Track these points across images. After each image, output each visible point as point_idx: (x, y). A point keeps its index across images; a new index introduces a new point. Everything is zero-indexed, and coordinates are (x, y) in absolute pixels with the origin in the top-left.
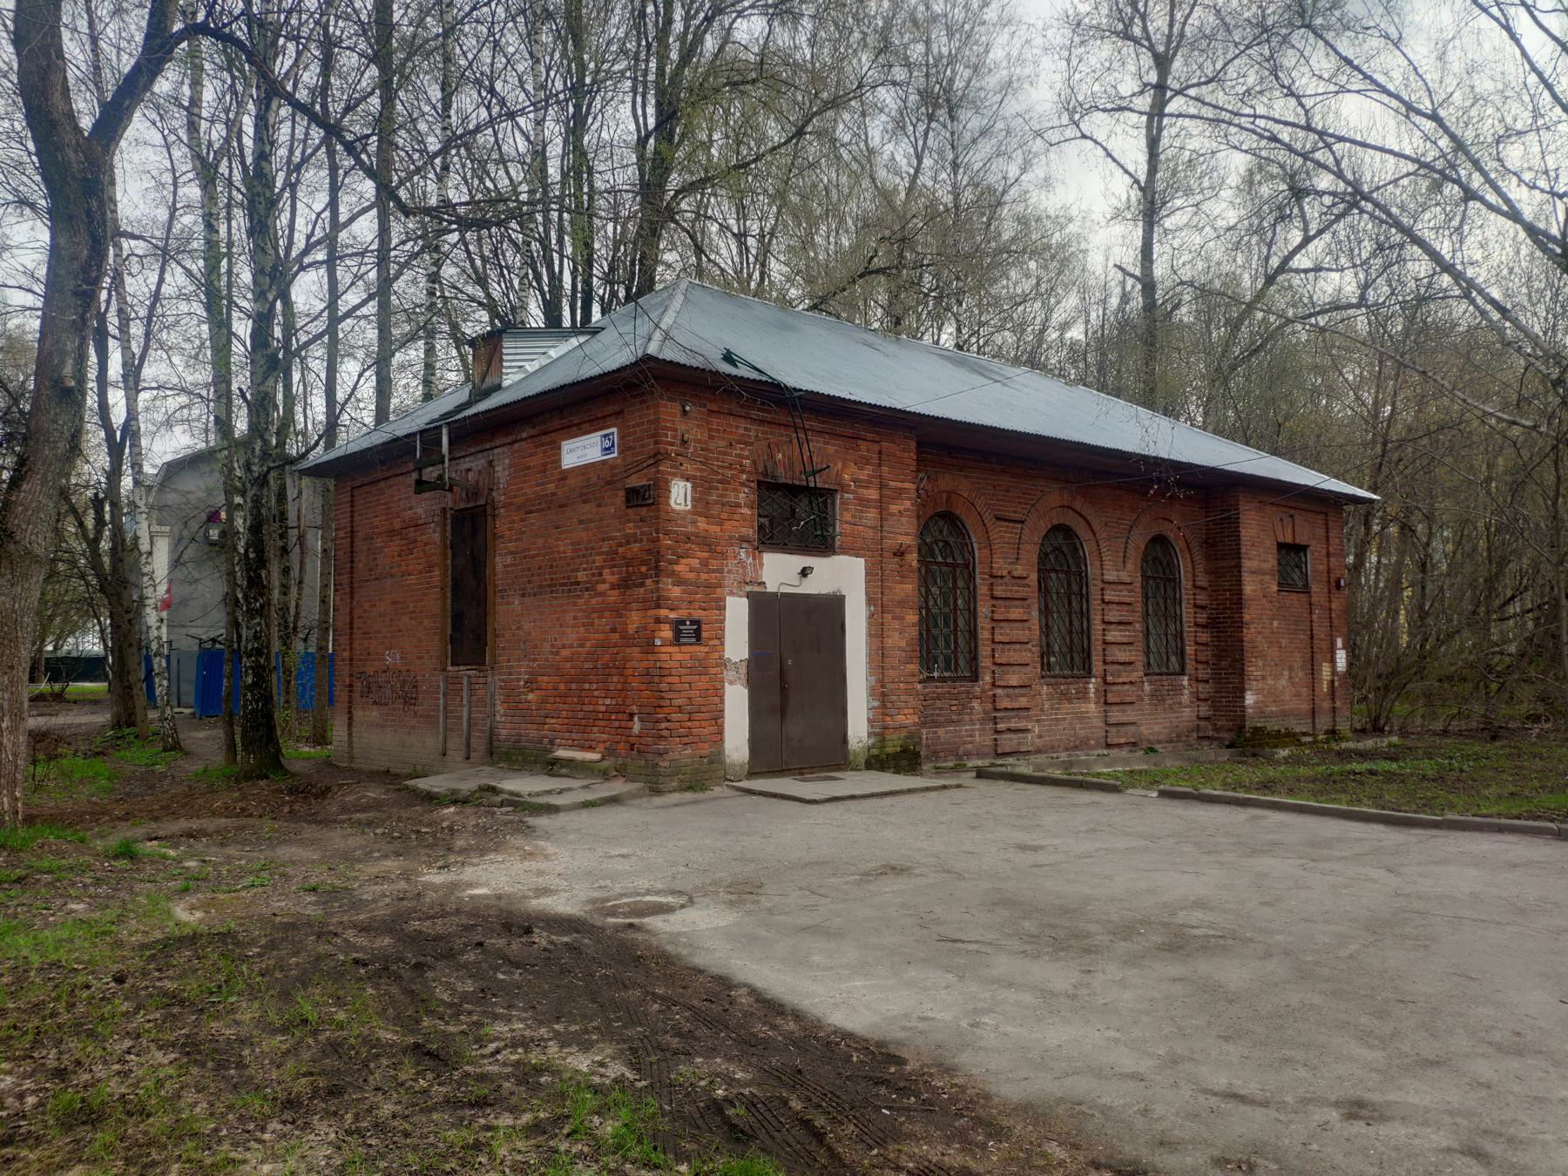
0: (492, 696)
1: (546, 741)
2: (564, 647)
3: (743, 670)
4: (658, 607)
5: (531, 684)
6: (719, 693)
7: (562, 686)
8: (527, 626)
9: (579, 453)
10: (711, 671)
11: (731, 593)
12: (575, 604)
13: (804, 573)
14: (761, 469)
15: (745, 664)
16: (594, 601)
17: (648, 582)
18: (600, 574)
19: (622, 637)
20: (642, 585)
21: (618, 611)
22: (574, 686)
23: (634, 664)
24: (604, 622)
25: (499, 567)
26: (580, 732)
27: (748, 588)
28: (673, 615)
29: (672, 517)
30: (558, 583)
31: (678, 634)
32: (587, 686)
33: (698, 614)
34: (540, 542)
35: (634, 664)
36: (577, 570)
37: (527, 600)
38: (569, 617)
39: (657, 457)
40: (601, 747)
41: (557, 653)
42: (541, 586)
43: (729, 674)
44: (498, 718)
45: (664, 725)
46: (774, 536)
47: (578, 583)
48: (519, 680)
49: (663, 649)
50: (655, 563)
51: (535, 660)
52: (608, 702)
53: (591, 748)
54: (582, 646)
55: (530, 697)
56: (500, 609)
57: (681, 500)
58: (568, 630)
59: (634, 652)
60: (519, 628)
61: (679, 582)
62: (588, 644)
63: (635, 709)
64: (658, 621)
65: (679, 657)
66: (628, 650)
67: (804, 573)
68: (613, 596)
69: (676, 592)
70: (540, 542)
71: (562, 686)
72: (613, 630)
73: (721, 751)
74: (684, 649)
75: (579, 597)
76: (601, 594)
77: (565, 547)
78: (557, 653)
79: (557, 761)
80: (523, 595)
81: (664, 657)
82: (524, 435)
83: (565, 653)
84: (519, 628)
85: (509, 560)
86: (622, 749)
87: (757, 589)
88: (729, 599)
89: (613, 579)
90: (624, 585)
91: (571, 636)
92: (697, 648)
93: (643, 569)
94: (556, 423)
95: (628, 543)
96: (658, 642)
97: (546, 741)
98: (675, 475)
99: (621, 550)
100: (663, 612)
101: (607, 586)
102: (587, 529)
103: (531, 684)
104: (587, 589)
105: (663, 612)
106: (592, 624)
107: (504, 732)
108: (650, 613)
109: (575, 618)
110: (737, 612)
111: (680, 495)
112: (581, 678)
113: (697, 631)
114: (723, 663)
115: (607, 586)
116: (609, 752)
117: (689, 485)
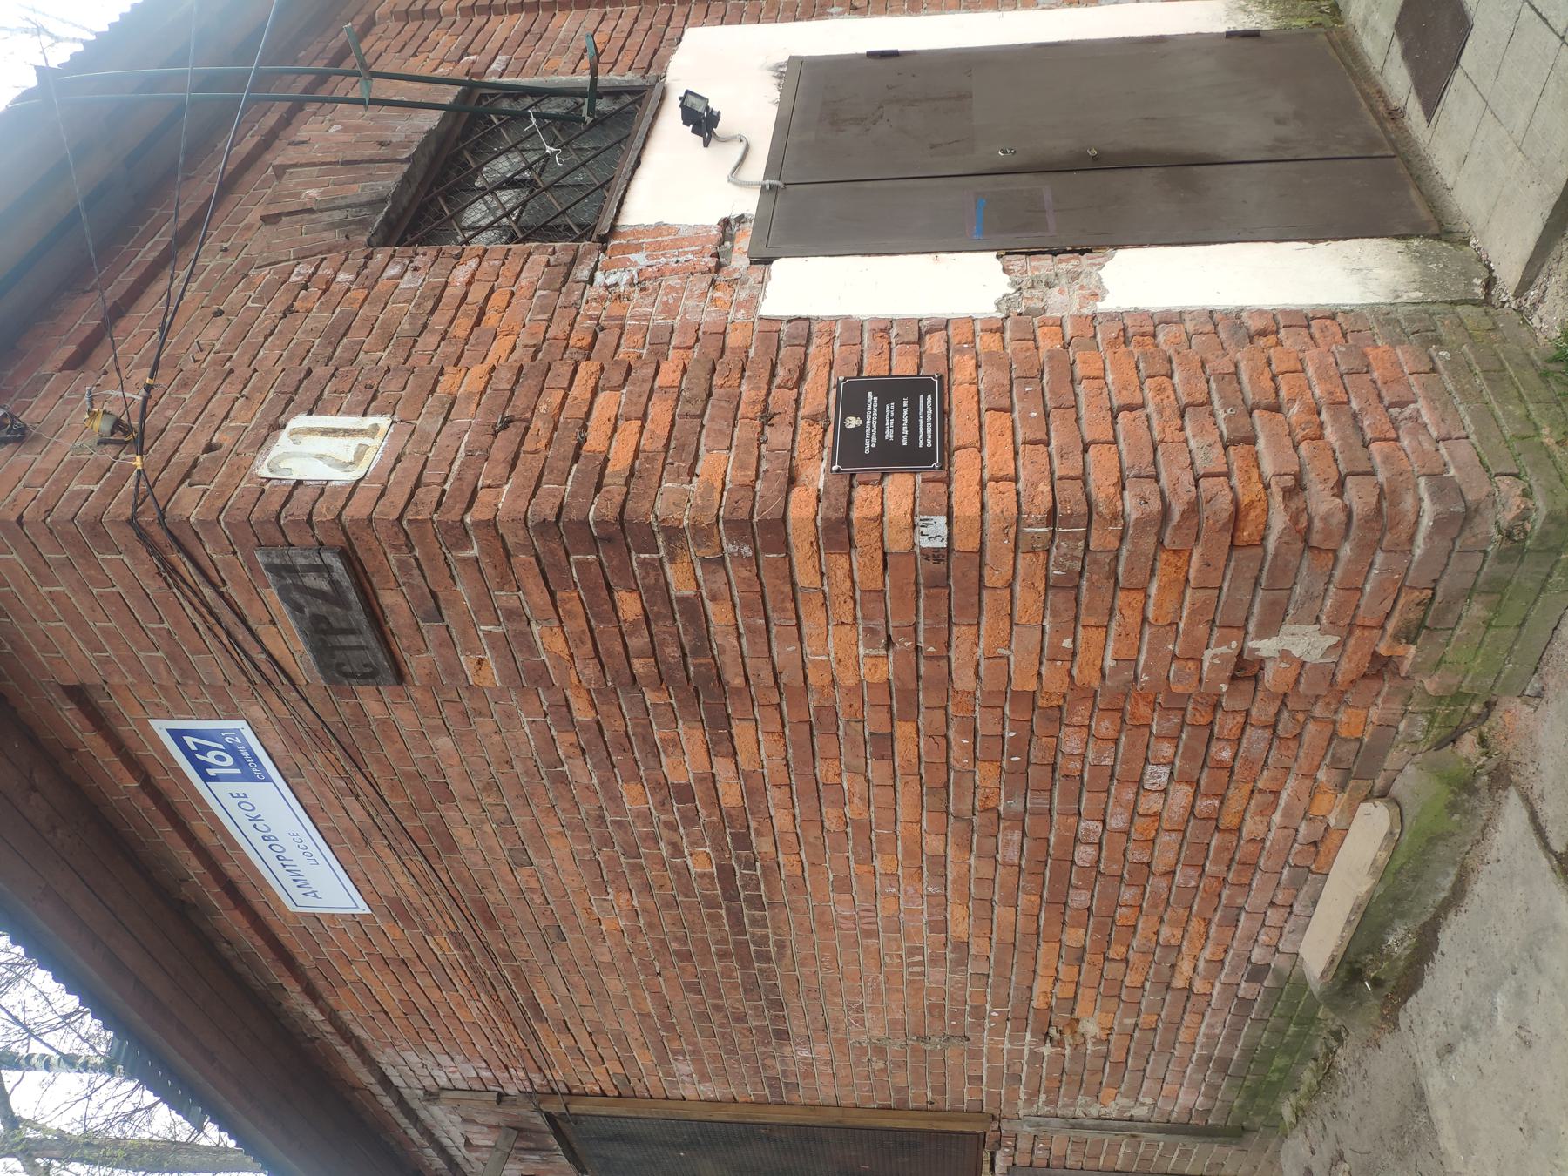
0: (1075, 1124)
1: (1245, 990)
2: (941, 926)
3: (1044, 265)
4: (776, 532)
5: (1052, 1025)
6: (1139, 330)
7: (1074, 936)
8: (875, 1029)
9: (301, 864)
10: (1038, 365)
11: (753, 302)
12: (798, 886)
13: (702, 121)
14: (335, 237)
15: (1017, 262)
16: (781, 820)
17: (679, 579)
18: (685, 793)
19: (911, 708)
20: (694, 610)
21: (812, 731)
22: (1079, 899)
23: (1021, 660)
24: (849, 775)
25: (707, 1090)
26: (1234, 870)
27: (739, 262)
28: (818, 474)
29: (408, 468)
30: (733, 927)
31: (901, 456)
32: (1084, 854)
33: (817, 394)
34: (615, 985)
35: (1021, 660)
36: (683, 872)
37: (796, 1027)
38: (840, 907)
39: (165, 542)
40: (1331, 808)
41: (962, 947)
42: (751, 988)
43: (1062, 303)
44: (1140, 1112)
45: (1321, 502)
46: (575, 210)
47: (726, 873)
48: (1036, 1057)
49: (966, 507)
50: (596, 548)
51: (979, 1013)
52: (1158, 775)
53: (1322, 847)
54: (940, 863)
55: (1090, 1027)
56: (825, 1092)
57: (343, 448)
58: (884, 908)
59: (970, 649)
60: (880, 1051)
61: (680, 452)
62: (933, 844)
63: (1216, 655)
64: (838, 532)
65: (998, 456)
66: (964, 680)
67: (702, 121)
68: (758, 743)
69: (719, 464)
70: (615, 985)
71: (1074, 936)
72: (884, 744)
73: (1385, 317)
74: (962, 429)
75: (772, 869)
76: (753, 789)
77: (616, 911)
78: (962, 947)
79: (1350, 972)
80: (783, 1035)
81: (1000, 502)
82: (315, 1015)
83: (960, 922)
84: (880, 1051)
85: (683, 1067)
86: (1360, 719)
87: (743, 243)
88: (769, 308)
89: (692, 737)
90: (707, 695)
91: (907, 901)
92: (960, 395)
93: (629, 606)
94: (233, 922)
95: (540, 676)
96: (934, 533)
97: (1245, 990)
98: (244, 469)
99: (583, 713)
100: (801, 508)
101: (723, 768)
102: (541, 838)
103: (1052, 1025)
104: (742, 841)
105: (801, 508)
106: (864, 828)
107: (1186, 1099)
108: (805, 576)
109: (843, 885)
110: (807, 287)
111: (323, 453)
112: (1052, 873)
113: (896, 407)
114: (1017, 322)
115: (723, 768)
116: (1362, 773)
117: (301, 421)
